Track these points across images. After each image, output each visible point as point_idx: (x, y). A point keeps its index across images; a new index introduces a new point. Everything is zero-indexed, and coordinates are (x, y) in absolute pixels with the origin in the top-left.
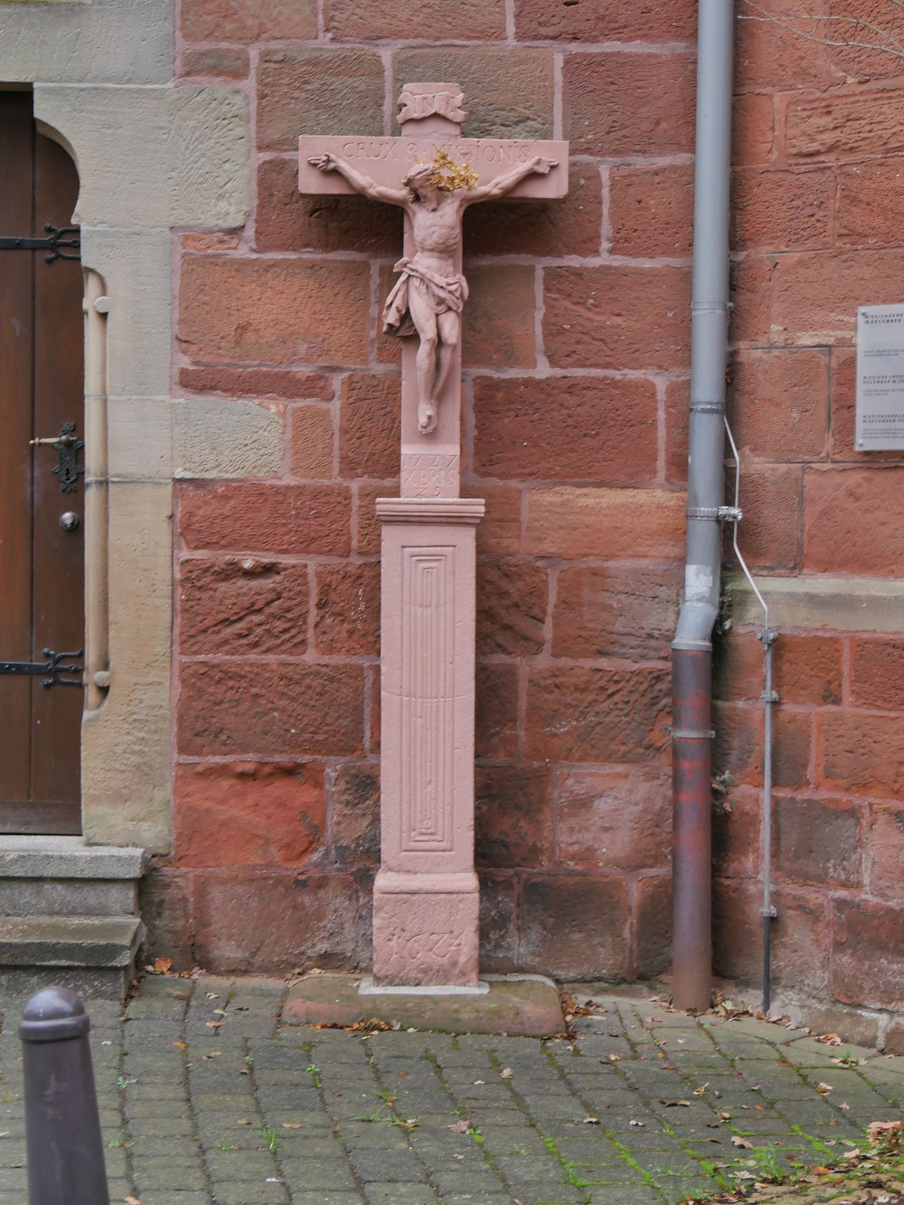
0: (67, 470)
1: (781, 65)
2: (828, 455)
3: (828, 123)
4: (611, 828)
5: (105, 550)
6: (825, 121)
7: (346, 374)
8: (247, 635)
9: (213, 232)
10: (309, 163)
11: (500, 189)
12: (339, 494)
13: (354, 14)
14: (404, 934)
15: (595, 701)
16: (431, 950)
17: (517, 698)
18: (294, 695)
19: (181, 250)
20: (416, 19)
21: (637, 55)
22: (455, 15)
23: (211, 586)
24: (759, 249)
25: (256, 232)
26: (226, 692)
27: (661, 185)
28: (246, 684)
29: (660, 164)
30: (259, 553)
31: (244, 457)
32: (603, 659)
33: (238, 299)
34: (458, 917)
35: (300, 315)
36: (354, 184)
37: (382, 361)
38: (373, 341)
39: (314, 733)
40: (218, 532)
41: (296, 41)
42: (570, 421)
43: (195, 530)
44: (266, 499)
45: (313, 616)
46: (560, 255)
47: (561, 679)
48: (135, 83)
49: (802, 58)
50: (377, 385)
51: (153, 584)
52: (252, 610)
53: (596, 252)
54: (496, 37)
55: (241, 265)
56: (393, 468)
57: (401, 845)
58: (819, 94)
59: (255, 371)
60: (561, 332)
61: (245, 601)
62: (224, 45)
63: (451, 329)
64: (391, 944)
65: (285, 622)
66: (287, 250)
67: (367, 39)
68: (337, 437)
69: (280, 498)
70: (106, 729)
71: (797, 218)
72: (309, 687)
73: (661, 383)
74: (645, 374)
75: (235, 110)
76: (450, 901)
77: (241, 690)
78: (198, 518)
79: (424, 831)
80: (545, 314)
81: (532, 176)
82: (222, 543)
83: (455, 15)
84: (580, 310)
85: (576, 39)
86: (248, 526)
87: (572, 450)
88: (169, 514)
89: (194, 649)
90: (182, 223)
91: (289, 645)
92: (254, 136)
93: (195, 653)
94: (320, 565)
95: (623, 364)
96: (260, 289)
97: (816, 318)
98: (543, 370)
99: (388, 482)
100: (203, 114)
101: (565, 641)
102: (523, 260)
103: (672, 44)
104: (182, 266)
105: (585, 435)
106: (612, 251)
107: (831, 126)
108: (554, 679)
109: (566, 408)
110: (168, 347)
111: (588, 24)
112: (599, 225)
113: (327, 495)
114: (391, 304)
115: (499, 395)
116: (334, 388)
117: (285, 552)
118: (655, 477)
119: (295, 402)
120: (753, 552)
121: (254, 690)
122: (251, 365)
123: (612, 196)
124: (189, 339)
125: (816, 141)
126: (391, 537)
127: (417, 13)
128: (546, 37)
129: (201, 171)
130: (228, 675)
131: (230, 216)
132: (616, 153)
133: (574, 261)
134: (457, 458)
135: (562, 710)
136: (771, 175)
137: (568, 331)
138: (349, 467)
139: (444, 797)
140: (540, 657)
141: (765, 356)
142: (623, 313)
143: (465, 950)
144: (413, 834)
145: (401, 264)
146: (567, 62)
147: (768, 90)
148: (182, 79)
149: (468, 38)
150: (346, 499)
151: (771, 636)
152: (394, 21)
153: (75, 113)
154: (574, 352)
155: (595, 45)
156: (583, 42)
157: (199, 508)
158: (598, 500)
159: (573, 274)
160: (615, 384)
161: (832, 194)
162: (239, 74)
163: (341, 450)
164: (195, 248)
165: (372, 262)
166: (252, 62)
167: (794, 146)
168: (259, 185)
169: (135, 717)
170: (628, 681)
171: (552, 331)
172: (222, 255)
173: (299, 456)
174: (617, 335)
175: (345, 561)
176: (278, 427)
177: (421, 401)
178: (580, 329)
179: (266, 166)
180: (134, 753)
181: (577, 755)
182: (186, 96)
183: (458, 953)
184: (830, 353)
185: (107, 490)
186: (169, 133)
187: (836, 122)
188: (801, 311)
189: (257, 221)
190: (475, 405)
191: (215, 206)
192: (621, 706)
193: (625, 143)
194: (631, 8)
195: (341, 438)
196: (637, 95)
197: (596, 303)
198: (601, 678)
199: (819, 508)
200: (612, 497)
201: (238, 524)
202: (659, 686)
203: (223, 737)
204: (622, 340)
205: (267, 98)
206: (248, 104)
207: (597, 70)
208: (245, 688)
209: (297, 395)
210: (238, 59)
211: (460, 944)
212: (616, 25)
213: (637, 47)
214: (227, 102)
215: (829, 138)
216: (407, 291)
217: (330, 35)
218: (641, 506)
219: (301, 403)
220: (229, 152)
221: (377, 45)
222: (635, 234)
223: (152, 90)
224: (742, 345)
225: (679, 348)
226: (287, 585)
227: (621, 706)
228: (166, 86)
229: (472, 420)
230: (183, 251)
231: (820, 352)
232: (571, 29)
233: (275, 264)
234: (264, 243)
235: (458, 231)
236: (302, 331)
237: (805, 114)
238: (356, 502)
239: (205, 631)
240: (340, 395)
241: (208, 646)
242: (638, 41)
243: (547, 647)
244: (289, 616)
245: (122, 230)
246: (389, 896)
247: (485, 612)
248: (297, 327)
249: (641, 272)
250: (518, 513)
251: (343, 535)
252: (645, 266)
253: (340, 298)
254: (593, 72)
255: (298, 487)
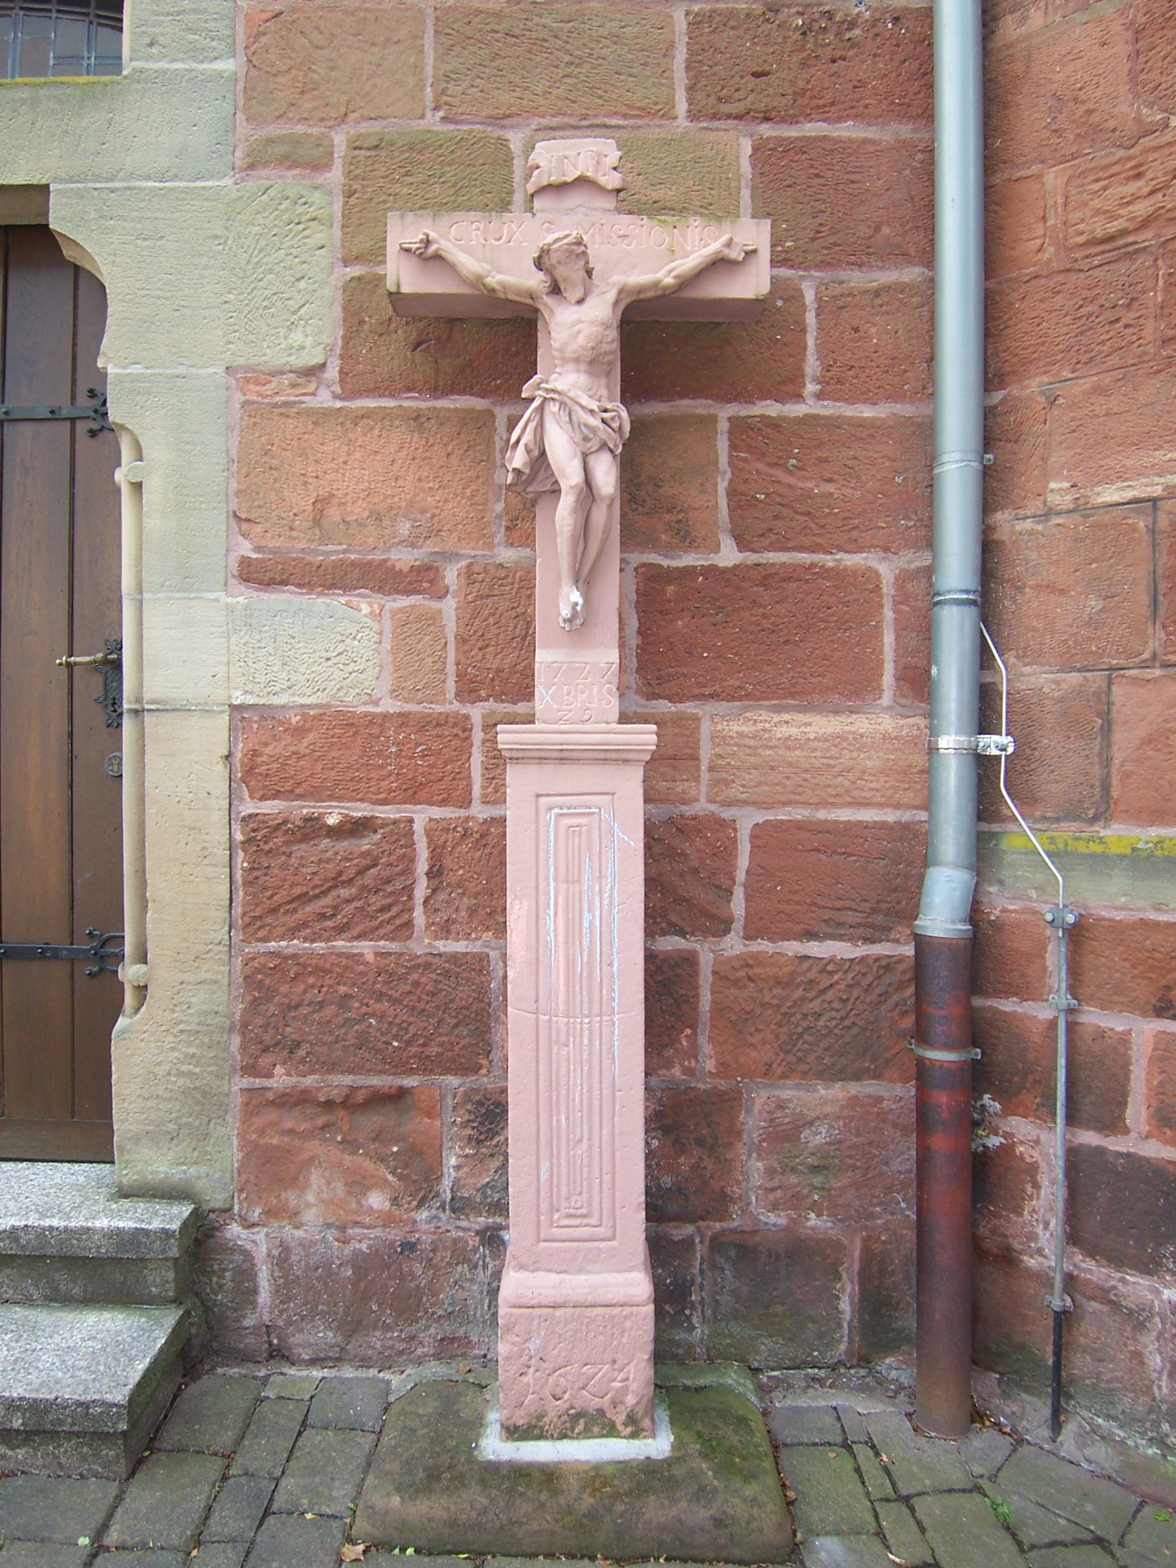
0: (114, 699)
1: (1055, 131)
2: (1154, 656)
3: (1140, 188)
4: (825, 1168)
5: (141, 800)
6: (1134, 187)
7: (464, 563)
8: (334, 915)
9: (282, 373)
10: (402, 248)
11: (675, 277)
12: (455, 725)
13: (473, 86)
14: (545, 1365)
15: (803, 999)
16: (583, 1388)
17: (697, 996)
18: (397, 995)
19: (239, 397)
20: (555, 92)
21: (851, 140)
22: (607, 87)
23: (283, 849)
24: (1026, 382)
25: (341, 372)
26: (305, 991)
27: (884, 308)
28: (332, 982)
29: (883, 281)
30: (349, 804)
31: (325, 675)
32: (812, 943)
33: (317, 462)
34: (624, 1340)
35: (401, 482)
36: (464, 272)
37: (512, 545)
38: (499, 517)
39: (424, 1045)
40: (292, 778)
41: (396, 120)
42: (765, 623)
43: (260, 774)
44: (356, 733)
45: (421, 890)
46: (750, 400)
47: (757, 970)
48: (181, 180)
49: (1090, 112)
50: (506, 577)
51: (204, 848)
52: (337, 881)
53: (799, 397)
54: (663, 116)
55: (322, 416)
56: (526, 692)
57: (539, 1236)
58: (1121, 153)
59: (341, 560)
60: (753, 503)
61: (331, 869)
62: (300, 129)
63: (606, 476)
64: (524, 1379)
65: (385, 897)
66: (382, 395)
67: (491, 117)
68: (451, 647)
69: (376, 731)
70: (143, 1044)
71: (1091, 329)
72: (416, 984)
73: (886, 569)
74: (865, 559)
75: (312, 212)
76: (612, 1317)
77: (324, 989)
78: (265, 758)
79: (572, 1211)
80: (731, 481)
81: (719, 265)
82: (297, 791)
83: (607, 87)
84: (779, 474)
85: (767, 119)
86: (332, 769)
87: (769, 663)
88: (226, 753)
89: (260, 934)
90: (242, 361)
91: (390, 927)
92: (339, 244)
93: (264, 940)
94: (431, 820)
95: (838, 546)
96: (346, 448)
97: (1129, 463)
98: (728, 555)
99: (521, 708)
100: (271, 218)
101: (761, 918)
102: (700, 407)
103: (894, 126)
104: (241, 419)
105: (786, 642)
106: (820, 396)
107: (1146, 190)
108: (748, 970)
109: (761, 606)
110: (223, 527)
111: (784, 101)
112: (803, 360)
113: (438, 725)
114: (518, 441)
115: (670, 590)
116: (447, 581)
117: (385, 802)
118: (880, 698)
119: (394, 600)
120: (1026, 799)
121: (342, 989)
122: (333, 552)
123: (819, 322)
124: (252, 516)
125: (1120, 216)
126: (518, 781)
127: (557, 85)
128: (729, 116)
129: (266, 292)
130: (303, 967)
131: (306, 350)
132: (823, 265)
133: (771, 409)
134: (615, 667)
135: (758, 1011)
136: (1043, 281)
137: (761, 502)
138: (468, 690)
139: (601, 1162)
140: (728, 938)
141: (1039, 527)
142: (836, 477)
143: (634, 1387)
144: (556, 1216)
145: (532, 385)
146: (756, 149)
147: (1035, 169)
148: (244, 174)
149: (625, 116)
150: (464, 730)
151: (1070, 919)
152: (528, 95)
153: (102, 221)
154: (770, 530)
155: (793, 127)
156: (777, 123)
157: (266, 744)
158: (803, 729)
159: (768, 425)
160: (824, 572)
161: (1150, 284)
162: (319, 165)
163: (457, 664)
164: (259, 395)
165: (497, 410)
166: (336, 149)
167: (1082, 233)
168: (345, 309)
169: (182, 1026)
170: (846, 971)
171: (740, 500)
172: (295, 402)
173: (401, 672)
174: (828, 507)
175: (462, 813)
176: (372, 634)
177: (563, 583)
178: (778, 499)
179: (353, 284)
180: (181, 1074)
181: (779, 1071)
182: (248, 195)
183: (624, 1390)
184: (1155, 508)
185: (143, 722)
186: (225, 242)
187: (1154, 183)
188: (1099, 456)
189: (342, 357)
190: (638, 602)
191: (286, 338)
192: (836, 1005)
193: (836, 253)
194: (841, 80)
195: (457, 650)
196: (850, 191)
197: (800, 464)
198: (809, 969)
199: (1142, 732)
200: (822, 725)
201: (319, 767)
202: (886, 980)
203: (301, 1053)
204: (836, 514)
205: (356, 196)
206: (331, 203)
207: (796, 158)
208: (330, 986)
209: (398, 592)
210: (318, 145)
211: (627, 1379)
212: (821, 102)
213: (848, 130)
214: (303, 200)
215: (1141, 209)
216: (541, 423)
217: (441, 114)
218: (862, 736)
219: (404, 602)
220: (305, 266)
221: (503, 127)
222: (850, 373)
223: (204, 188)
224: (1001, 517)
225: (911, 524)
226: (386, 847)
227: (836, 1005)
228: (223, 183)
229: (633, 623)
230: (243, 399)
231: (1137, 511)
232: (761, 106)
233: (367, 414)
234: (351, 386)
235: (614, 334)
236: (403, 504)
237: (1097, 186)
238: (478, 736)
239: (274, 911)
240: (455, 591)
241: (280, 930)
242: (850, 123)
243: (738, 925)
244: (389, 889)
245: (161, 371)
246: (522, 1310)
247: (654, 880)
248: (396, 499)
249: (861, 423)
250: (697, 748)
251: (460, 779)
252: (866, 415)
253: (454, 459)
254: (792, 161)
255: (400, 714)
